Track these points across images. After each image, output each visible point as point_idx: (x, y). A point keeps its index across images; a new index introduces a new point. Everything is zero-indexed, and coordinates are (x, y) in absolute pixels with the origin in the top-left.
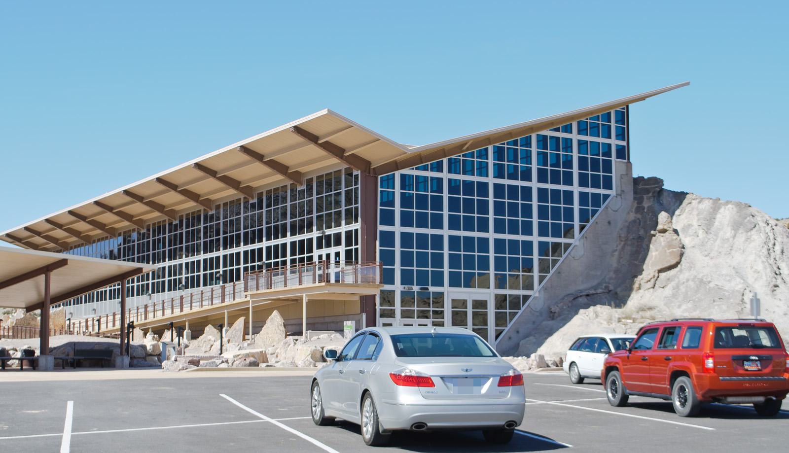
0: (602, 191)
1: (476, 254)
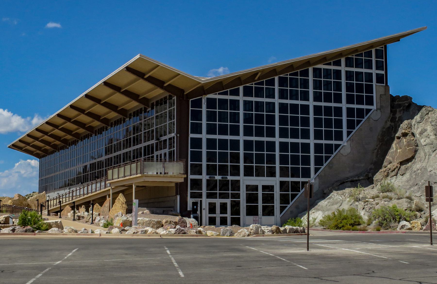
0: (365, 107)
1: (254, 152)
